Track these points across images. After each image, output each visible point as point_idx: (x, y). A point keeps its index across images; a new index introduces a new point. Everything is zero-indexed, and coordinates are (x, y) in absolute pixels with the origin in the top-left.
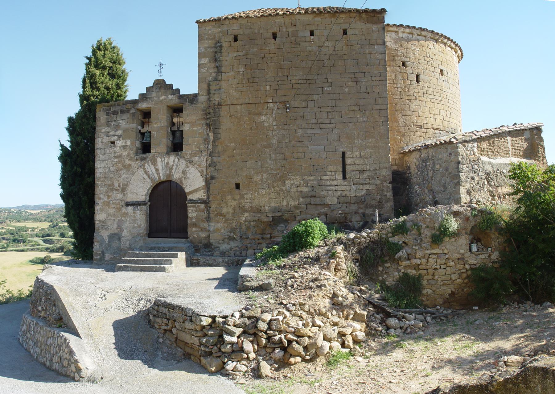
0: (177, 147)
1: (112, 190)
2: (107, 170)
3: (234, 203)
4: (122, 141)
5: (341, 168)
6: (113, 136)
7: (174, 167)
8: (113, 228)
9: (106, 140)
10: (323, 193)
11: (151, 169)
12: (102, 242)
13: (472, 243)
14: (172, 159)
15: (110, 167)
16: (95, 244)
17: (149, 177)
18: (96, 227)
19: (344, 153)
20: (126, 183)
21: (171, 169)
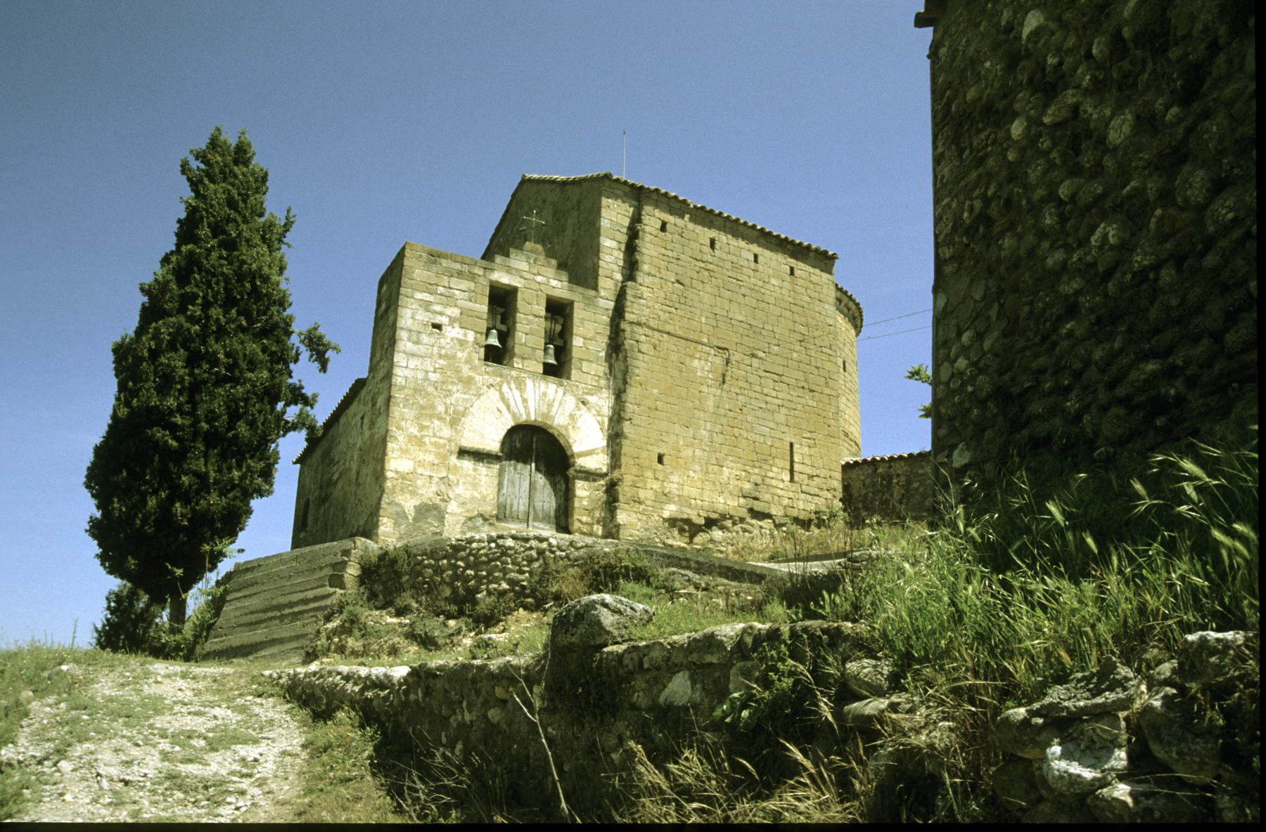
0: (557, 369)
1: (431, 417)
2: (420, 375)
3: (656, 485)
4: (457, 329)
5: (788, 467)
6: (441, 314)
7: (556, 404)
8: (428, 492)
9: (423, 316)
10: (767, 497)
11: (513, 395)
12: (400, 516)
13: (842, 674)
14: (551, 387)
15: (427, 372)
16: (384, 520)
17: (508, 408)
18: (388, 484)
19: (791, 445)
20: (461, 409)
21: (550, 405)
